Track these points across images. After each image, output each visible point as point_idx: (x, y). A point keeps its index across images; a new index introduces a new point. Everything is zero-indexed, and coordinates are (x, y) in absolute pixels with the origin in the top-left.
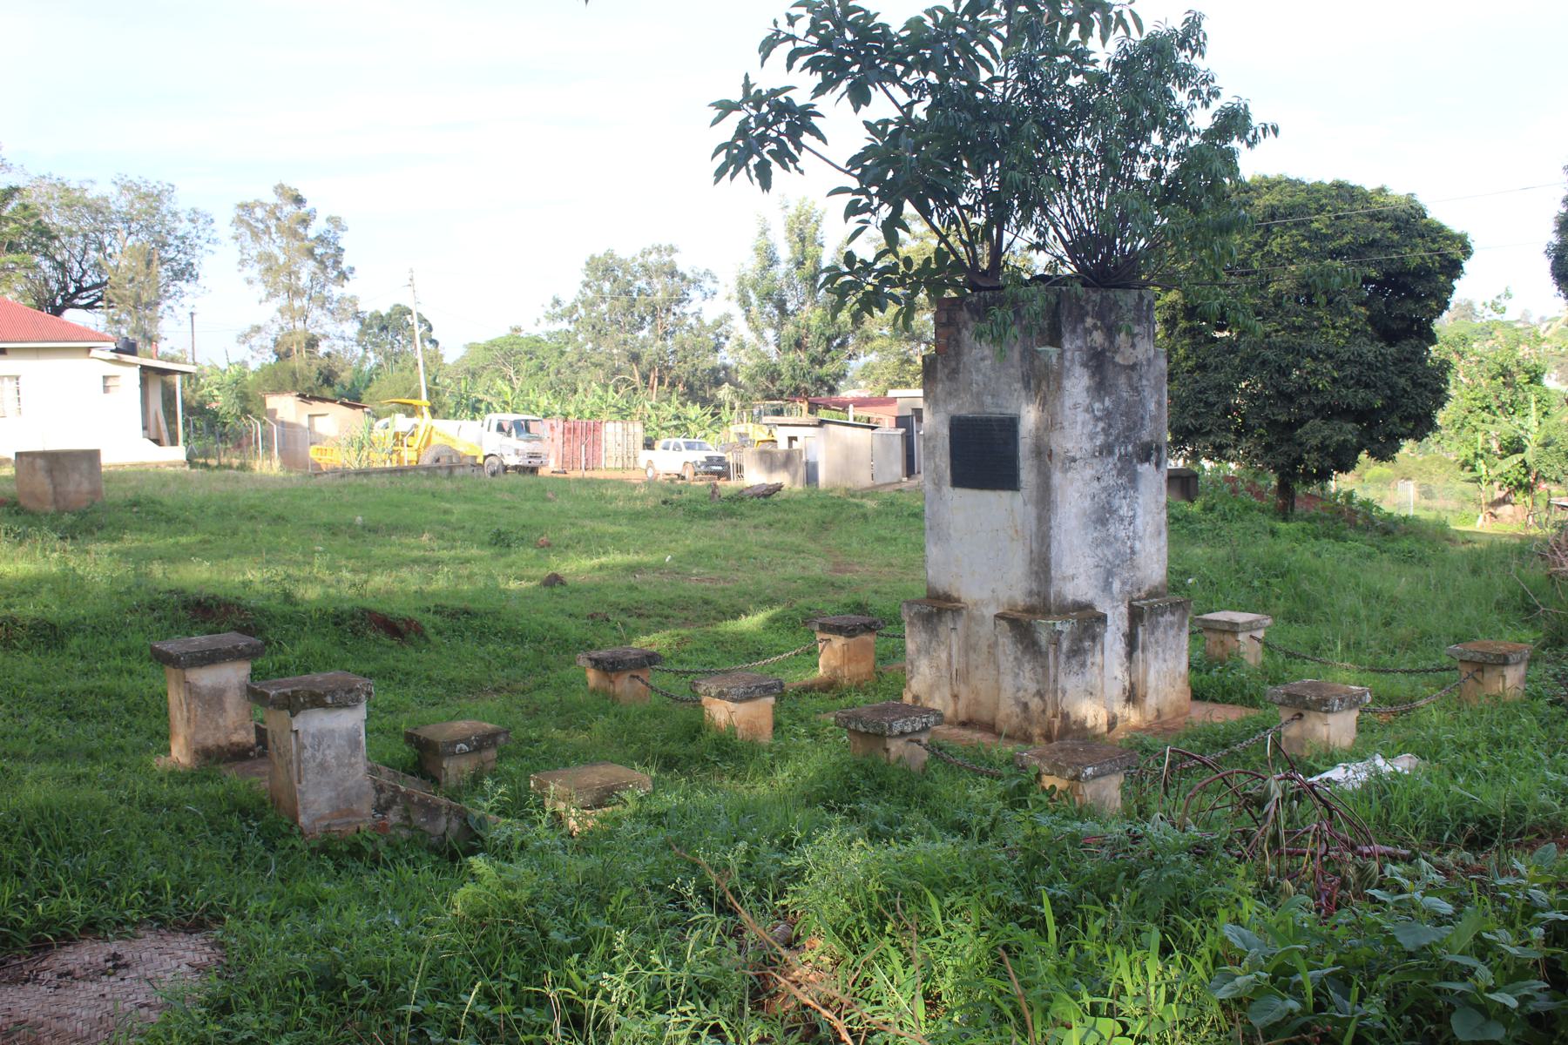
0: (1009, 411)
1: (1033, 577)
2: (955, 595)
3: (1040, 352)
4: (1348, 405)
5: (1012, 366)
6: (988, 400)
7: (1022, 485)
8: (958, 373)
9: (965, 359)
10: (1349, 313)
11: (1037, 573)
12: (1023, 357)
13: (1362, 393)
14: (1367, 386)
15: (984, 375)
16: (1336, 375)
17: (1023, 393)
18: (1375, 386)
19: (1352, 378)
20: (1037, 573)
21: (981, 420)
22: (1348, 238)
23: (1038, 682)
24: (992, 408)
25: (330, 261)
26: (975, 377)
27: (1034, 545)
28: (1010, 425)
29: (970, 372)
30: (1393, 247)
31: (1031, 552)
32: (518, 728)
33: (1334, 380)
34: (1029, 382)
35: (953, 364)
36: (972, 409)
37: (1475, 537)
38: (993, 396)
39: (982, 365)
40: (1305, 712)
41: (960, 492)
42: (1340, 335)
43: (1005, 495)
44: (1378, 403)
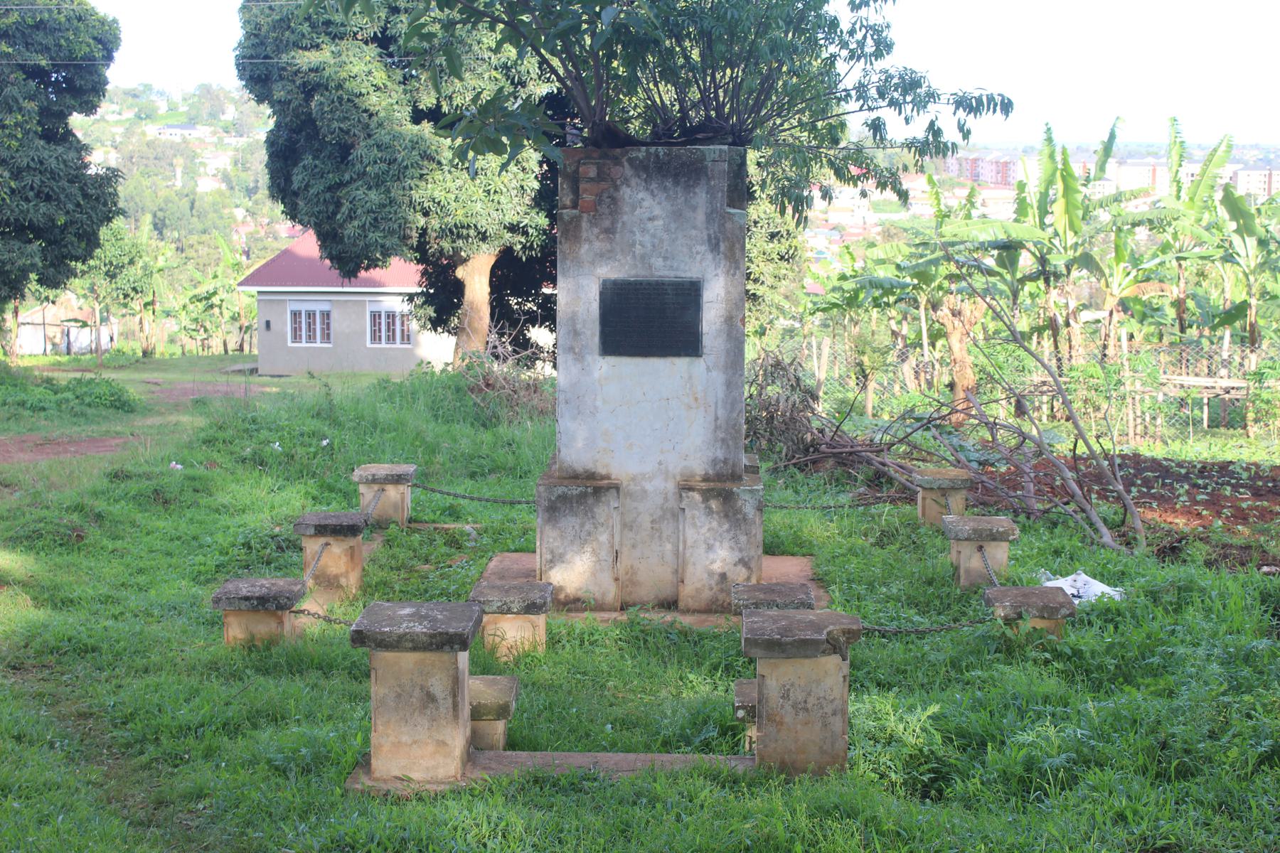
0: (689, 275)
1: (719, 445)
2: (603, 471)
3: (733, 215)
4: (30, 221)
5: (695, 228)
6: (658, 262)
7: (705, 351)
8: (614, 233)
9: (625, 218)
10: (20, 109)
11: (723, 440)
12: (709, 218)
13: (43, 207)
14: (48, 198)
15: (654, 236)
16: (13, 184)
17: (710, 256)
18: (58, 199)
19: (32, 188)
20: (723, 440)
21: (649, 283)
22: (14, 17)
23: (741, 550)
24: (661, 270)
25: (1032, 148)
26: (638, 237)
27: (721, 413)
28: (691, 293)
29: (632, 232)
30: (60, 30)
31: (717, 419)
32: (1195, 594)
33: (13, 191)
34: (717, 245)
35: (607, 223)
36: (633, 272)
37: (133, 385)
38: (665, 258)
39: (650, 225)
40: (985, 544)
41: (612, 360)
42: (11, 136)
43: (680, 365)
44: (61, 220)
